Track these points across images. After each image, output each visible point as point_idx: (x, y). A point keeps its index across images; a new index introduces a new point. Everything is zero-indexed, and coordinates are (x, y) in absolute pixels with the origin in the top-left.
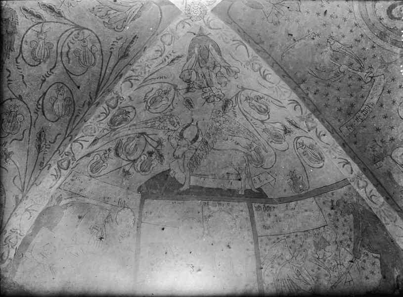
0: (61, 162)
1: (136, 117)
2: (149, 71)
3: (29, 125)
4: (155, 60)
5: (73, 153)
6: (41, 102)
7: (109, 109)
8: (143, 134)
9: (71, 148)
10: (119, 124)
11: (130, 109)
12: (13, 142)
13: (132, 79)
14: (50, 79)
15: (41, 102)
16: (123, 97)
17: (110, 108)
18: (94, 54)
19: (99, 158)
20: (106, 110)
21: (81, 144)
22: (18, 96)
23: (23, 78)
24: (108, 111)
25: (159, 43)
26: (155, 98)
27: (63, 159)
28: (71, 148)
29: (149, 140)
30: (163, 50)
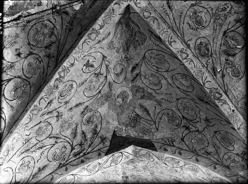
0: (215, 97)
1: (206, 37)
2: (167, 29)
3: (193, 102)
4: (160, 24)
5: (212, 88)
6: (182, 91)
7: (188, 59)
8: (225, 33)
9: (208, 88)
10: (208, 50)
11: (199, 41)
12: (200, 114)
13: (171, 41)
14: (170, 81)
15: (182, 91)
16: (181, 48)
17: (188, 58)
18: (158, 55)
19: (230, 69)
20: (188, 61)
21: (207, 82)
22: (176, 100)
23: (167, 94)
24: (189, 60)
25: (148, 20)
26: (197, 21)
27: (214, 95)
28: (208, 88)
29: (233, 29)
30: (153, 18)
